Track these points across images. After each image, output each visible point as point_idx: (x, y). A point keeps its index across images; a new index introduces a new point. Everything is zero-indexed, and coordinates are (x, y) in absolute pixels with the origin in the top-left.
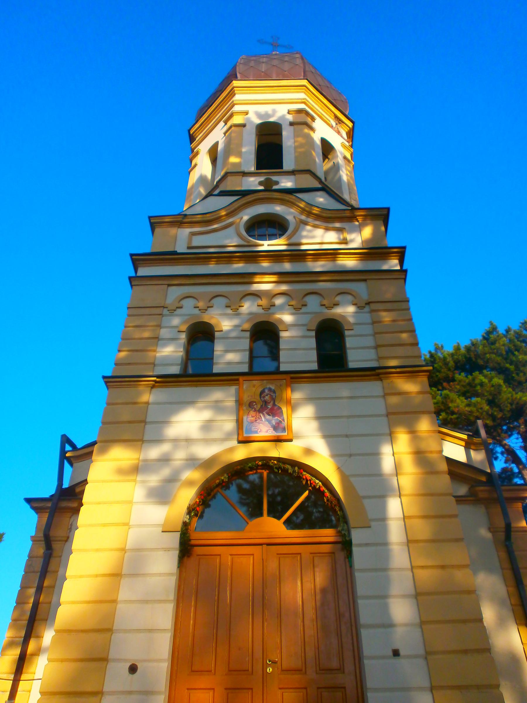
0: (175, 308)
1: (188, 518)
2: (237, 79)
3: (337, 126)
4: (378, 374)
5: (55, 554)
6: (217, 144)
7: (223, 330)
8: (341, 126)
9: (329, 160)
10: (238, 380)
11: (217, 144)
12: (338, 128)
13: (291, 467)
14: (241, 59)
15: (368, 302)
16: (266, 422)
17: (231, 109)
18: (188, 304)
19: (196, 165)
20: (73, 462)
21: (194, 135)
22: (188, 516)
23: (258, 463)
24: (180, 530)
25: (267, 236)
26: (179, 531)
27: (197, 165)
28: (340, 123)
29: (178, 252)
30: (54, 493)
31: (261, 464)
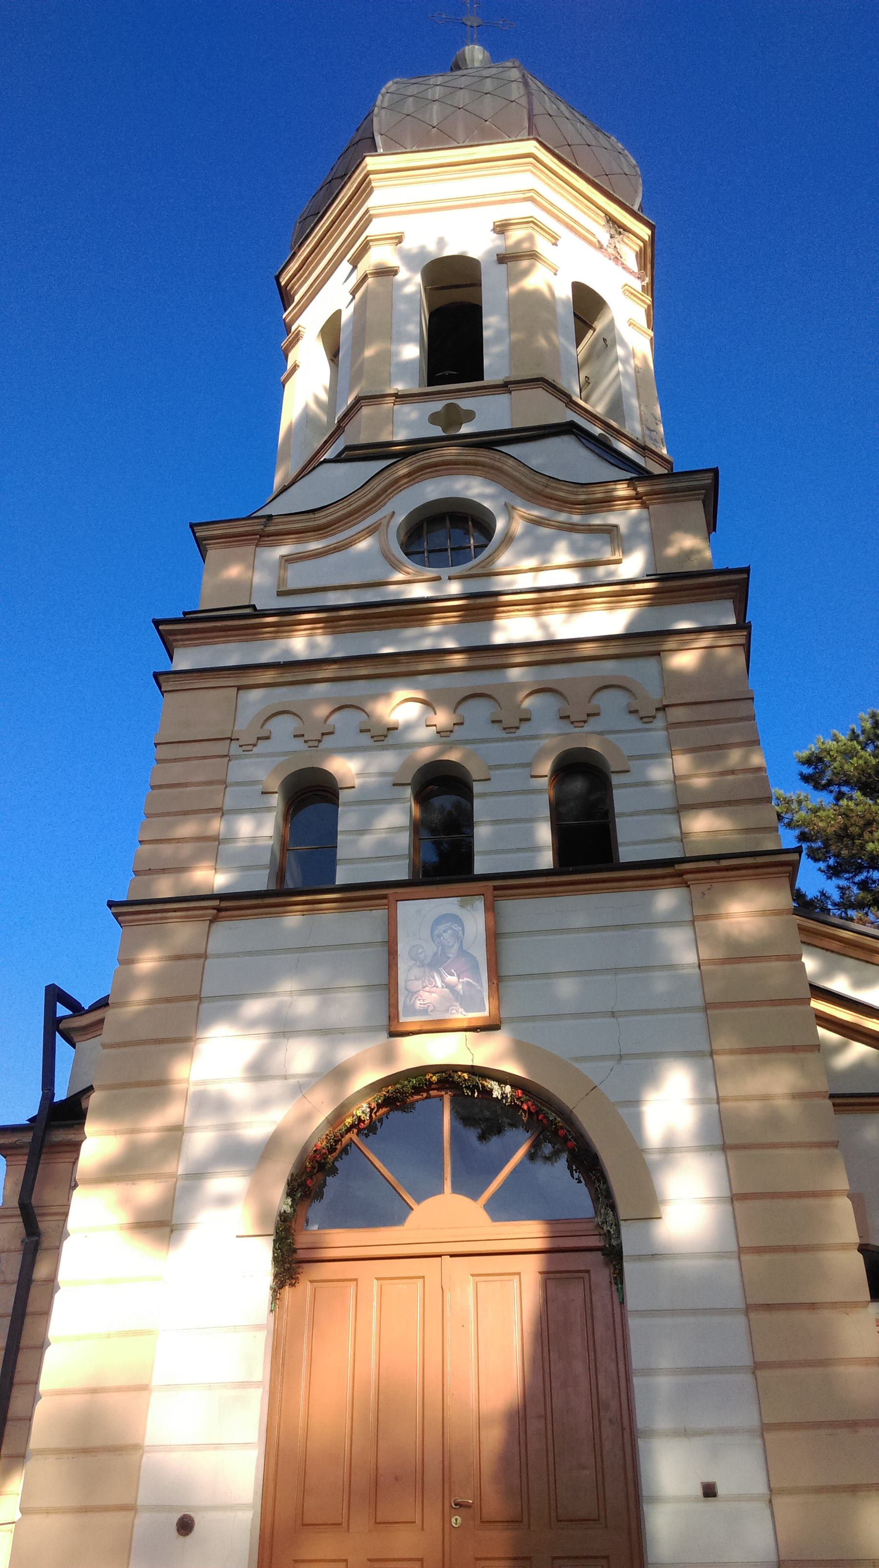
0: (254, 741)
1: (290, 1203)
2: (377, 153)
3: (612, 241)
4: (680, 874)
5: (46, 1243)
6: (338, 313)
7: (356, 786)
8: (623, 241)
9: (594, 332)
10: (385, 897)
11: (338, 313)
12: (615, 247)
13: (499, 1085)
14: (383, 96)
15: (660, 706)
16: (446, 989)
17: (362, 233)
18: (283, 727)
19: (295, 367)
20: (75, 1040)
21: (288, 288)
22: (289, 1201)
23: (431, 1077)
24: (272, 1233)
25: (449, 550)
26: (272, 1235)
27: (298, 366)
28: (620, 233)
29: (286, 484)
30: (37, 1113)
31: (436, 1080)
